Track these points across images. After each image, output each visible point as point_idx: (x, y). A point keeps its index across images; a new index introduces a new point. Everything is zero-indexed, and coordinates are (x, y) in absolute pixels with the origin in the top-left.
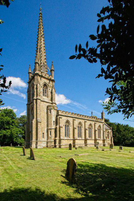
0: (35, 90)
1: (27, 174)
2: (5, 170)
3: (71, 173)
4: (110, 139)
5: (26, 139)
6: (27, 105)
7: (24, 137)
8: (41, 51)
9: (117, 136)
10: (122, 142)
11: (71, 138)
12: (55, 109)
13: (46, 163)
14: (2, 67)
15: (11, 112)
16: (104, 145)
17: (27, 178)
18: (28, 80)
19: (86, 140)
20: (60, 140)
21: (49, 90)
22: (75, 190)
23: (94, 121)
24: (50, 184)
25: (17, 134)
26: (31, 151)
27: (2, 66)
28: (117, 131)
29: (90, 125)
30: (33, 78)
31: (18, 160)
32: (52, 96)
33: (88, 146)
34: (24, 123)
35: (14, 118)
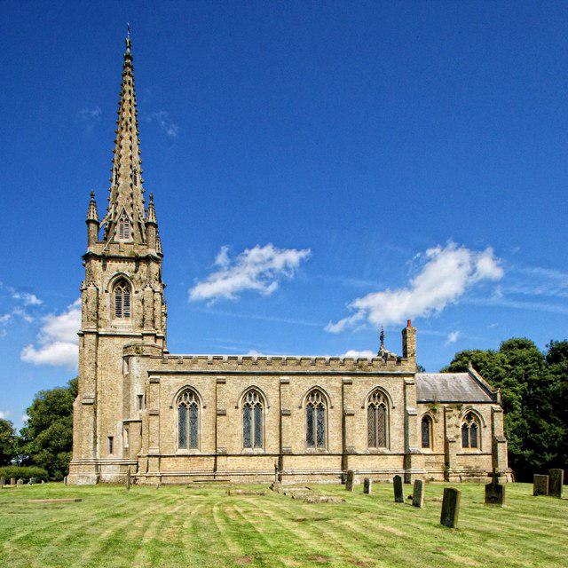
4: (489, 450)
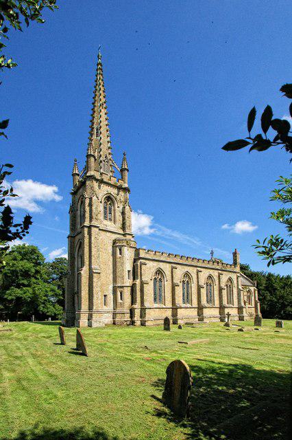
0: (87, 209)
1: (71, 393)
2: (19, 380)
3: (177, 394)
4: (253, 306)
5: (66, 306)
6: (68, 237)
7: (61, 303)
8: (101, 133)
9: (268, 298)
10: (280, 311)
11: (169, 305)
12: (131, 247)
13: (115, 363)
14: (6, 169)
15: (33, 251)
16: (241, 319)
17: (70, 402)
18: (71, 189)
19: (200, 308)
20: (143, 310)
21: (118, 207)
22: (189, 434)
23: (217, 269)
24: (128, 421)
25: (46, 296)
26: (79, 335)
27: (10, 166)
28: (267, 288)
29: (210, 277)
30: (83, 184)
31: (48, 355)
32: (124, 219)
33: (205, 320)
34: (61, 273)
35: (39, 264)
